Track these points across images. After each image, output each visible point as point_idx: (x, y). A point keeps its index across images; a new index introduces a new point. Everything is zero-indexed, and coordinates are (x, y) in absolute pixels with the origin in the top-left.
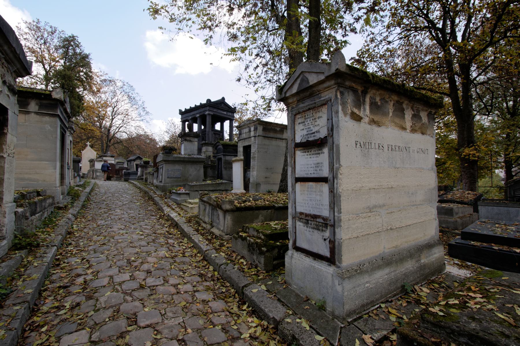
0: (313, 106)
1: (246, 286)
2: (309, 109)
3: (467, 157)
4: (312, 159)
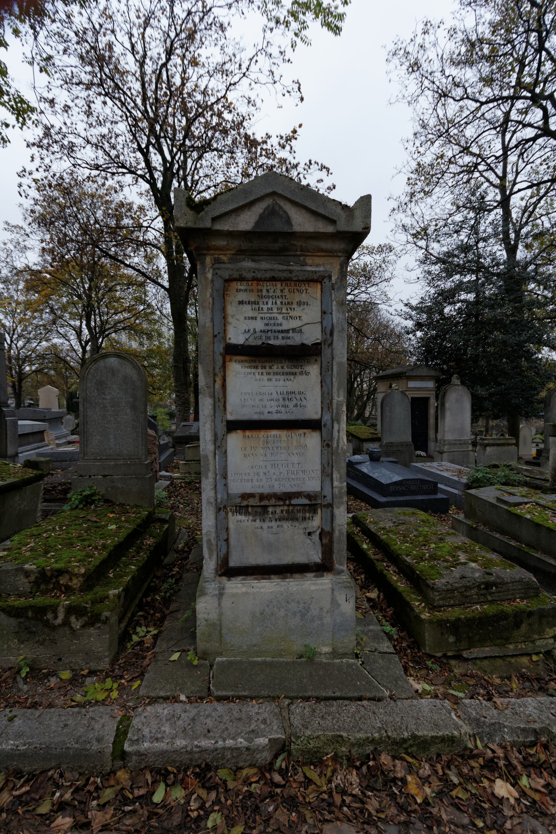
1: (121, 734)
2: (273, 279)
4: (274, 382)
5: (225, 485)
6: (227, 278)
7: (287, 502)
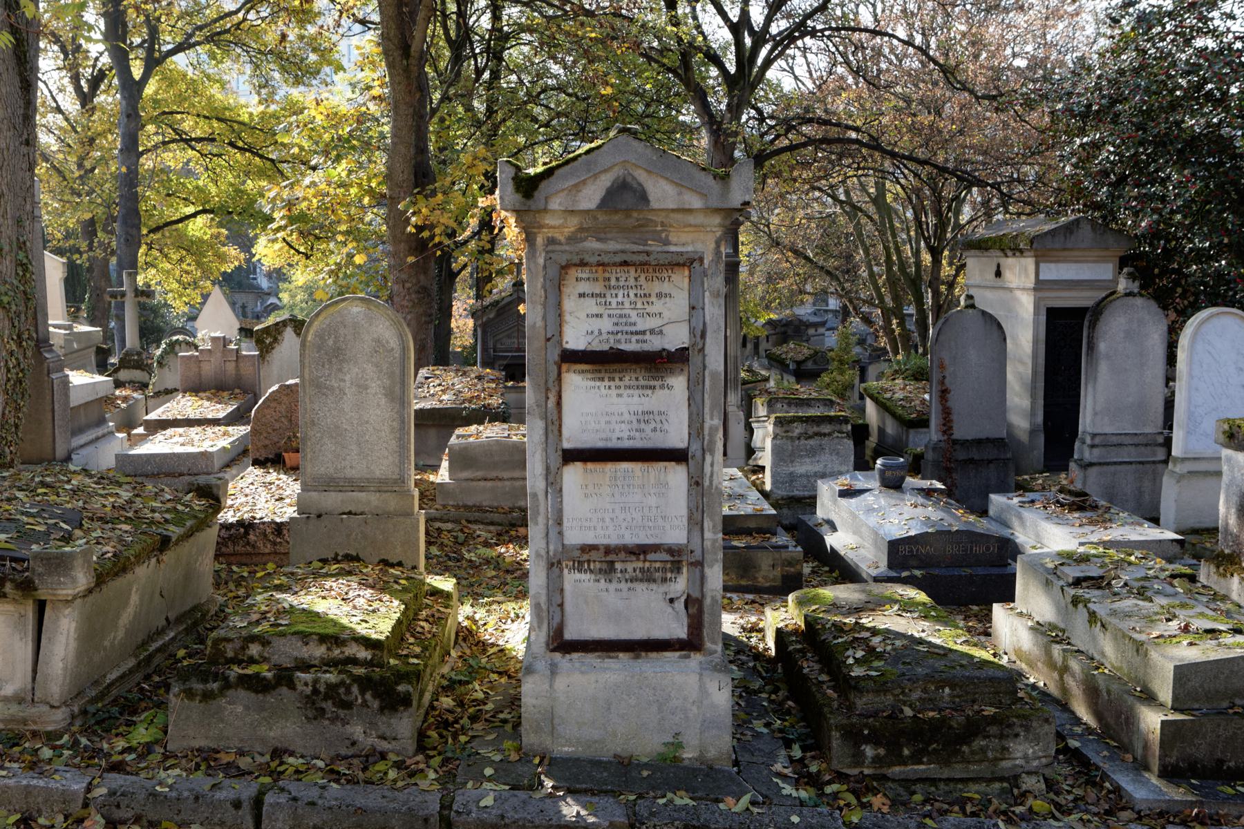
3: (426, 234)
4: (625, 399)
6: (564, 264)
7: (642, 557)
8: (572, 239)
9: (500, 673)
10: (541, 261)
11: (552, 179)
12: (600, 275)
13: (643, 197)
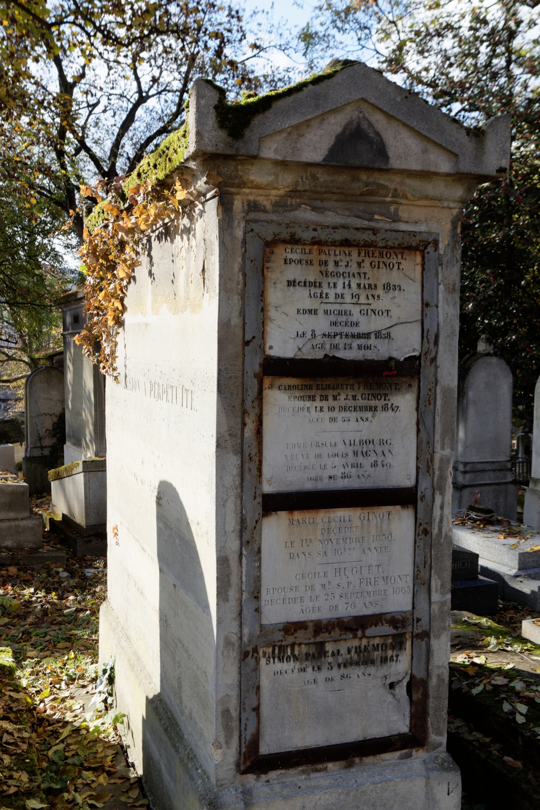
0: (367, 237)
2: (346, 243)
5: (258, 610)
6: (269, 238)
7: (359, 633)
8: (280, 206)
9: (94, 770)
10: (239, 233)
11: (270, 114)
12: (315, 256)
13: (381, 151)
